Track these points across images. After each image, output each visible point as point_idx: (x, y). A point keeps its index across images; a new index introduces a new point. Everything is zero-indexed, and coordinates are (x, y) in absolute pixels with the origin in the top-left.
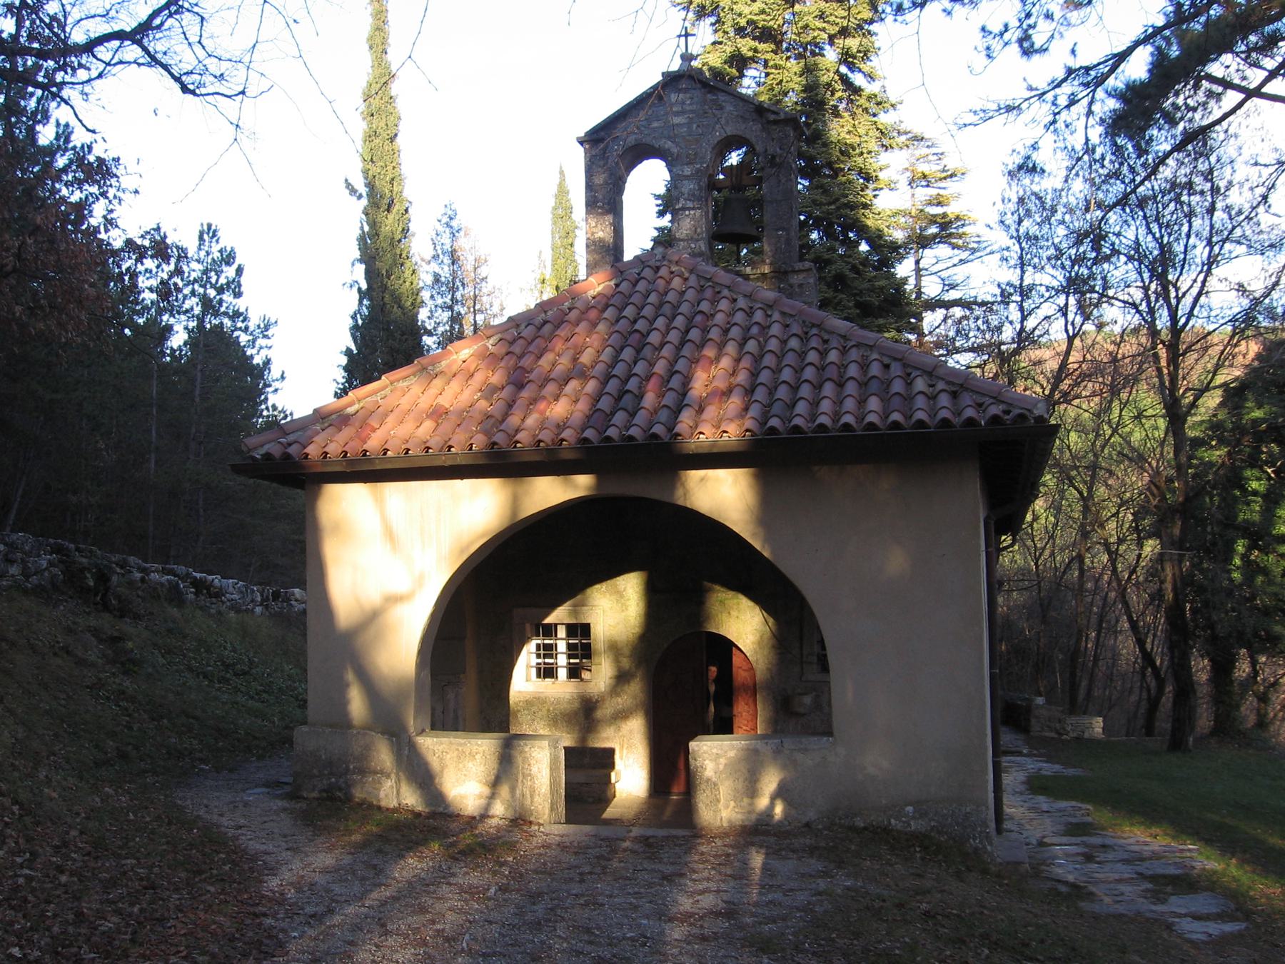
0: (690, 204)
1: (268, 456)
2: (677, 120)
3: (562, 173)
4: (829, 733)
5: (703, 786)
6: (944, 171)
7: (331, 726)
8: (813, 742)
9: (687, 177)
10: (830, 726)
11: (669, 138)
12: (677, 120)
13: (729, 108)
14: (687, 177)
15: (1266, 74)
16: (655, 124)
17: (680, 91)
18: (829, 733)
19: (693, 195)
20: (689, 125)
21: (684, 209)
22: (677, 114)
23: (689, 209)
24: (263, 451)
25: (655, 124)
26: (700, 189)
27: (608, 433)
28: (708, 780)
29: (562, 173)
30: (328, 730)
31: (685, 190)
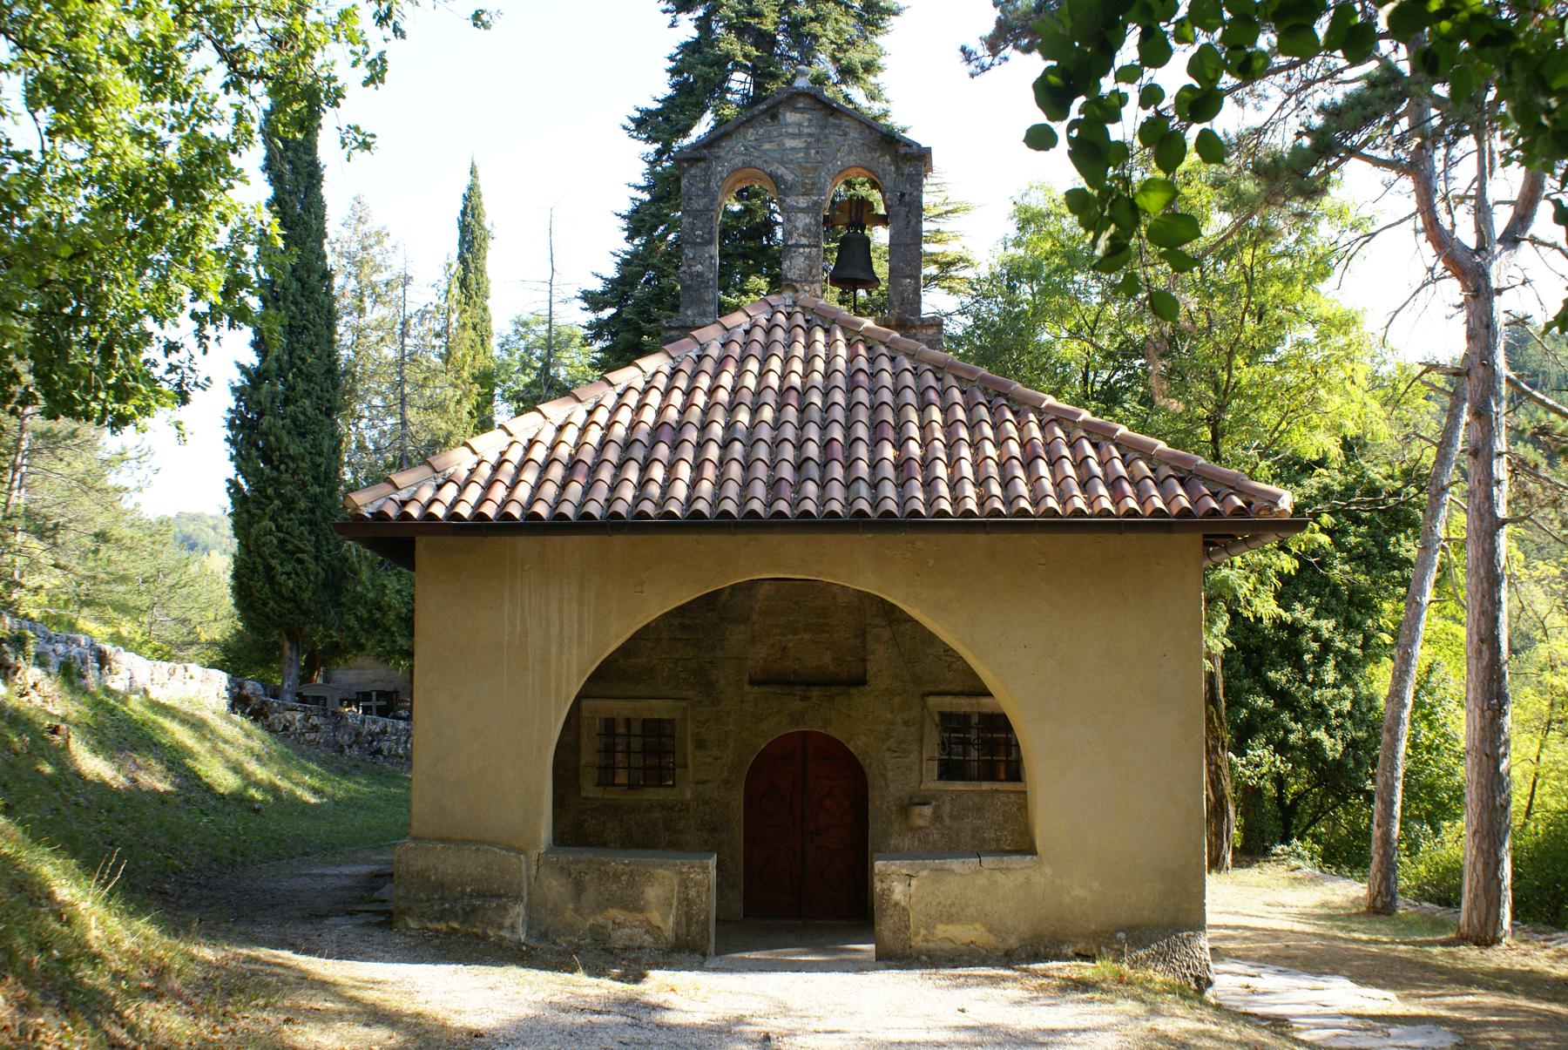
0: (804, 241)
1: (380, 515)
2: (789, 143)
3: (473, 172)
4: (1027, 847)
5: (890, 912)
6: (945, 203)
7: (441, 840)
8: (1015, 861)
9: (802, 210)
10: (1032, 844)
11: (783, 163)
12: (789, 143)
13: (853, 134)
14: (802, 210)
15: (1475, 155)
16: (767, 146)
17: (795, 110)
18: (1027, 847)
19: (809, 230)
20: (807, 149)
21: (798, 246)
22: (793, 136)
23: (803, 246)
24: (372, 509)
25: (767, 146)
26: (817, 224)
27: (721, 508)
28: (897, 904)
29: (473, 172)
30: (440, 846)
31: (800, 224)
